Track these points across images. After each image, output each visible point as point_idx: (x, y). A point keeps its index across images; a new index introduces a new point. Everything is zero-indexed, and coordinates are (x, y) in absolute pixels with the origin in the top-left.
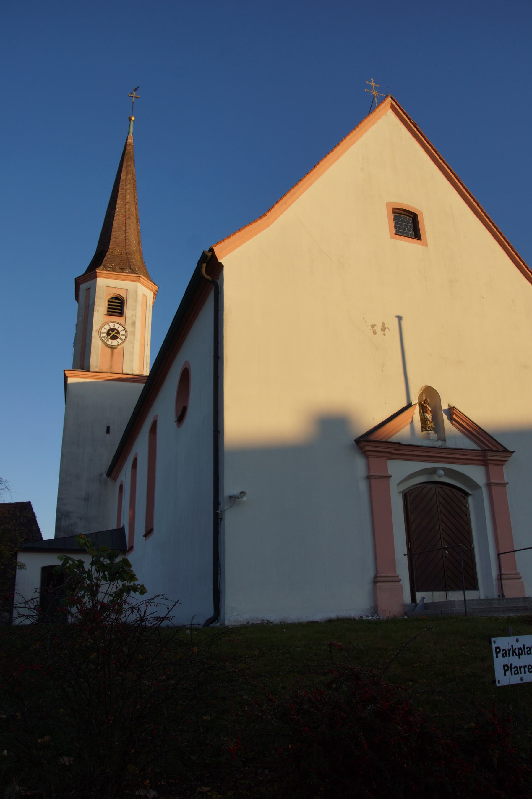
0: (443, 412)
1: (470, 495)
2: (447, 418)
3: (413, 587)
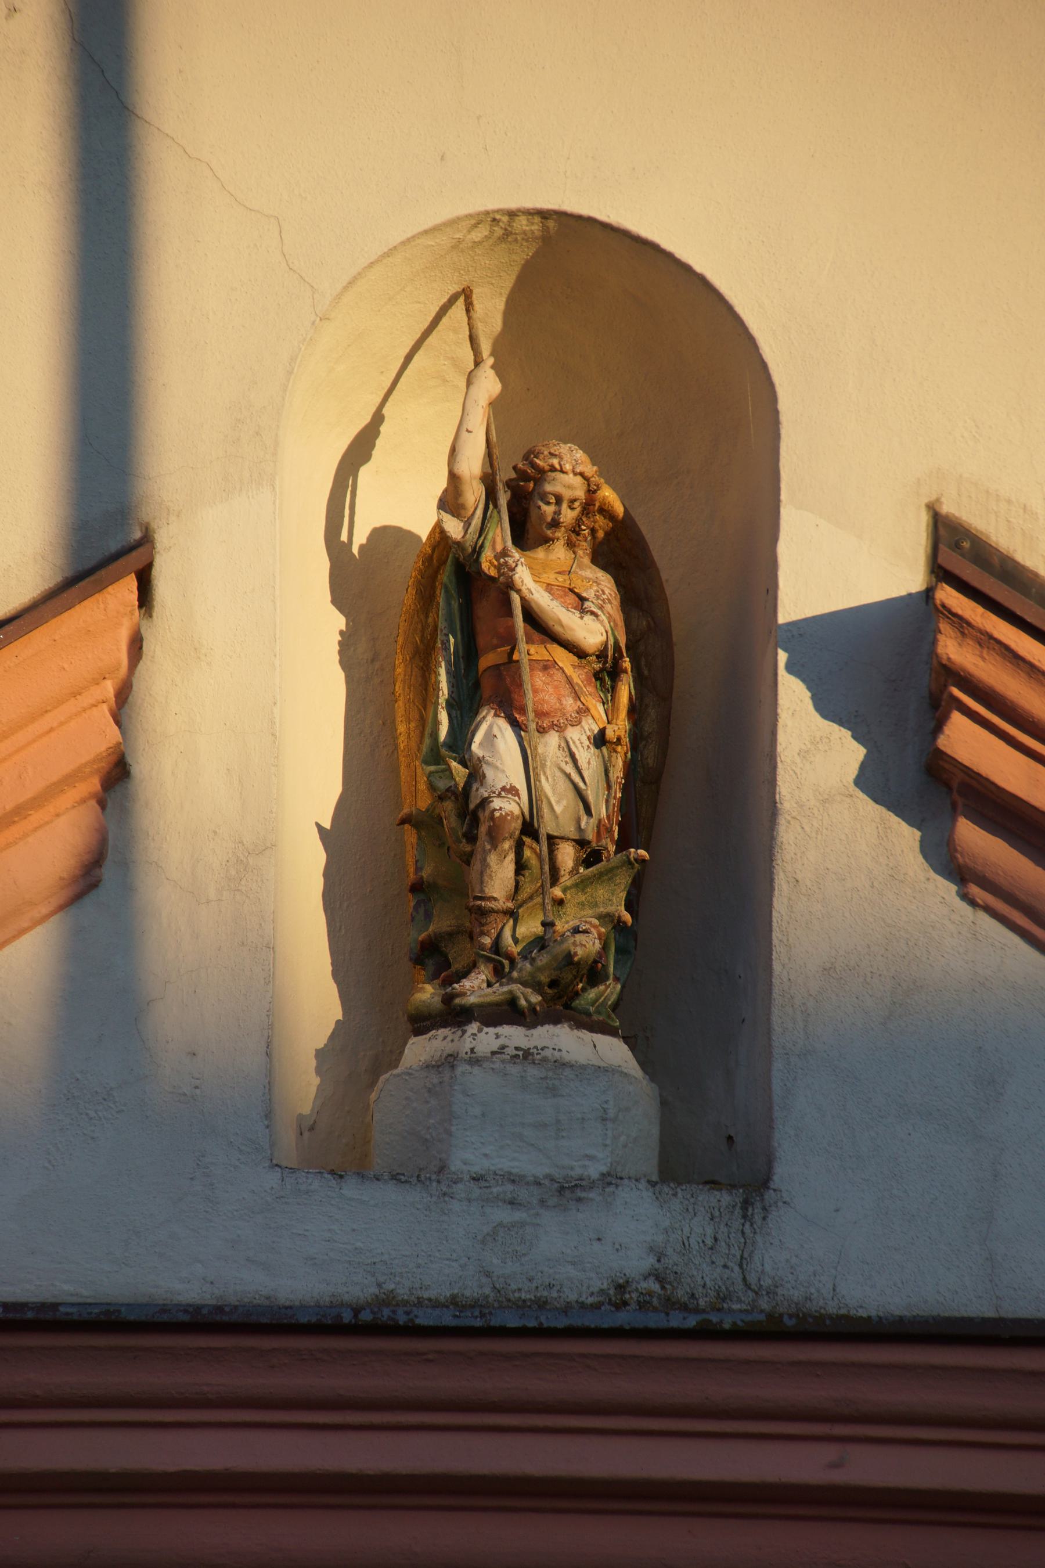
0: (790, 668)
2: (863, 781)
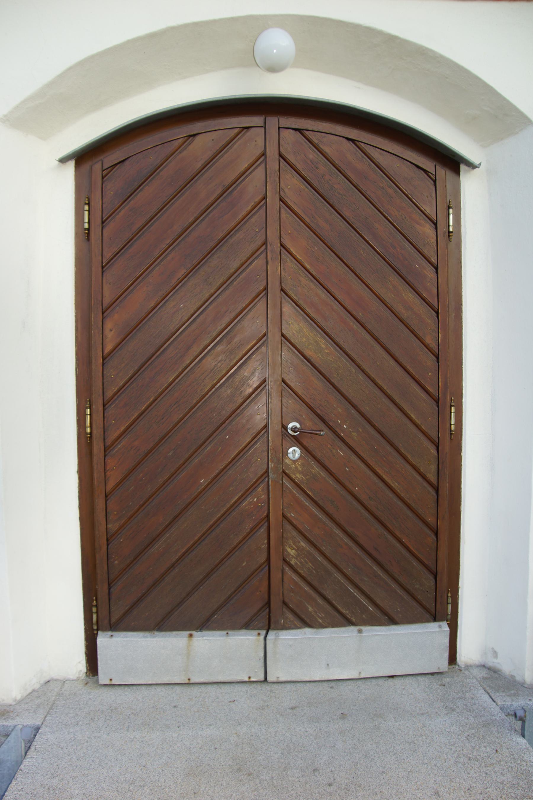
1: (472, 166)
3: (94, 610)
